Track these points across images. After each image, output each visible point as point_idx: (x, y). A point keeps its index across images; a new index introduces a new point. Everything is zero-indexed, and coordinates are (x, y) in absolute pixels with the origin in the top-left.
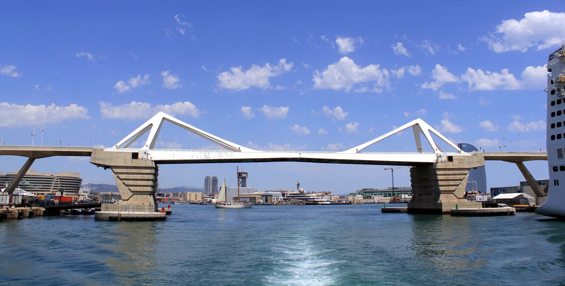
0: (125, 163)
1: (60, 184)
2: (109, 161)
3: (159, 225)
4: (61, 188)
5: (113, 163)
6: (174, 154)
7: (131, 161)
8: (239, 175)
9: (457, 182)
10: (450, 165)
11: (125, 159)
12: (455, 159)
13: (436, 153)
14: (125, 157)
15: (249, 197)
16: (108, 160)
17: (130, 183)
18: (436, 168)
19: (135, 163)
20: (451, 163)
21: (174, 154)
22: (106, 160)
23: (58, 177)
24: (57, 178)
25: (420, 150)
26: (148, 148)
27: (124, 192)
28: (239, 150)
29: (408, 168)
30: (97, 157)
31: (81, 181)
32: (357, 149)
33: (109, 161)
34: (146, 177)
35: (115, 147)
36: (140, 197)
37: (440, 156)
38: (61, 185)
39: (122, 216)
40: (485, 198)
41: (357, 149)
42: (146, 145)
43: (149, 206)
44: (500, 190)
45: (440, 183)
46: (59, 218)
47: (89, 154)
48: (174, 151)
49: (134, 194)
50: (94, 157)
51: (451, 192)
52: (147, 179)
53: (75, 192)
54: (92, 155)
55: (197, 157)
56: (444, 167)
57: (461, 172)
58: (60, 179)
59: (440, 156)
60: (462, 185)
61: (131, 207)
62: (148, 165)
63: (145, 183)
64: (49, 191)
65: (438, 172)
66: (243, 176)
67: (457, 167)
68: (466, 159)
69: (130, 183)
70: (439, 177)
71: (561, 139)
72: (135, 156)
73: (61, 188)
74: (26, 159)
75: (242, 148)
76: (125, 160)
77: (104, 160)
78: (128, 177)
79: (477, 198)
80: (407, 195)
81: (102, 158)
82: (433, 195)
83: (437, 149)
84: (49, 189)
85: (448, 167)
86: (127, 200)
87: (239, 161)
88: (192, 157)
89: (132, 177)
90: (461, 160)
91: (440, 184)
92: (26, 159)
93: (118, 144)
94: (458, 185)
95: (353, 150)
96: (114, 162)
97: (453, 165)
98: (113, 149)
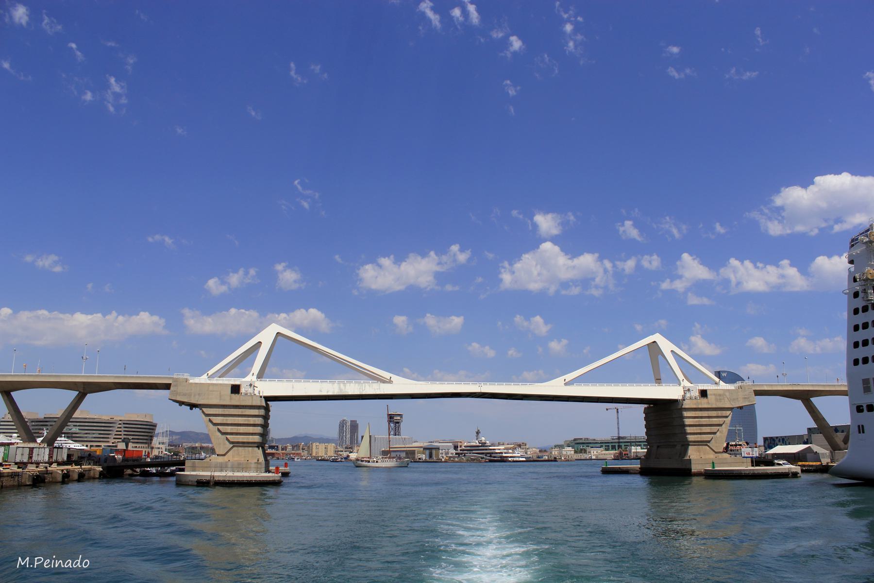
1: (125, 431)
2: (197, 397)
3: (271, 491)
4: (125, 437)
6: (293, 386)
7: (229, 398)
8: (390, 418)
9: (714, 429)
10: (704, 403)
12: (711, 395)
13: (682, 385)
14: (220, 391)
16: (195, 396)
17: (229, 429)
18: (683, 407)
19: (236, 400)
20: (704, 400)
21: (293, 386)
22: (192, 396)
23: (121, 420)
24: (120, 422)
25: (658, 381)
26: (255, 376)
27: (219, 443)
28: (390, 381)
29: (641, 408)
31: (156, 426)
32: (565, 380)
33: (197, 397)
34: (252, 420)
35: (205, 376)
36: (243, 451)
37: (689, 390)
38: (126, 433)
39: (216, 479)
40: (756, 452)
41: (565, 380)
43: (256, 464)
45: (689, 430)
47: (167, 387)
49: (233, 446)
50: (175, 391)
51: (705, 443)
53: (146, 443)
54: (172, 388)
55: (328, 392)
56: (695, 407)
57: (720, 413)
58: (124, 424)
59: (689, 390)
60: (720, 432)
61: (229, 466)
62: (254, 404)
63: (251, 429)
64: (108, 442)
65: (686, 414)
66: (396, 420)
67: (714, 406)
68: (727, 394)
69: (229, 429)
70: (687, 421)
72: (236, 389)
73: (125, 437)
74: (73, 394)
75: (395, 378)
78: (225, 420)
79: (744, 452)
81: (187, 392)
82: (678, 447)
84: (108, 438)
85: (700, 406)
86: (224, 455)
89: (230, 420)
90: (720, 395)
91: (688, 431)
92: (73, 394)
93: (211, 372)
94: (715, 433)
95: (560, 381)
96: (204, 399)
97: (708, 403)
98: (203, 379)
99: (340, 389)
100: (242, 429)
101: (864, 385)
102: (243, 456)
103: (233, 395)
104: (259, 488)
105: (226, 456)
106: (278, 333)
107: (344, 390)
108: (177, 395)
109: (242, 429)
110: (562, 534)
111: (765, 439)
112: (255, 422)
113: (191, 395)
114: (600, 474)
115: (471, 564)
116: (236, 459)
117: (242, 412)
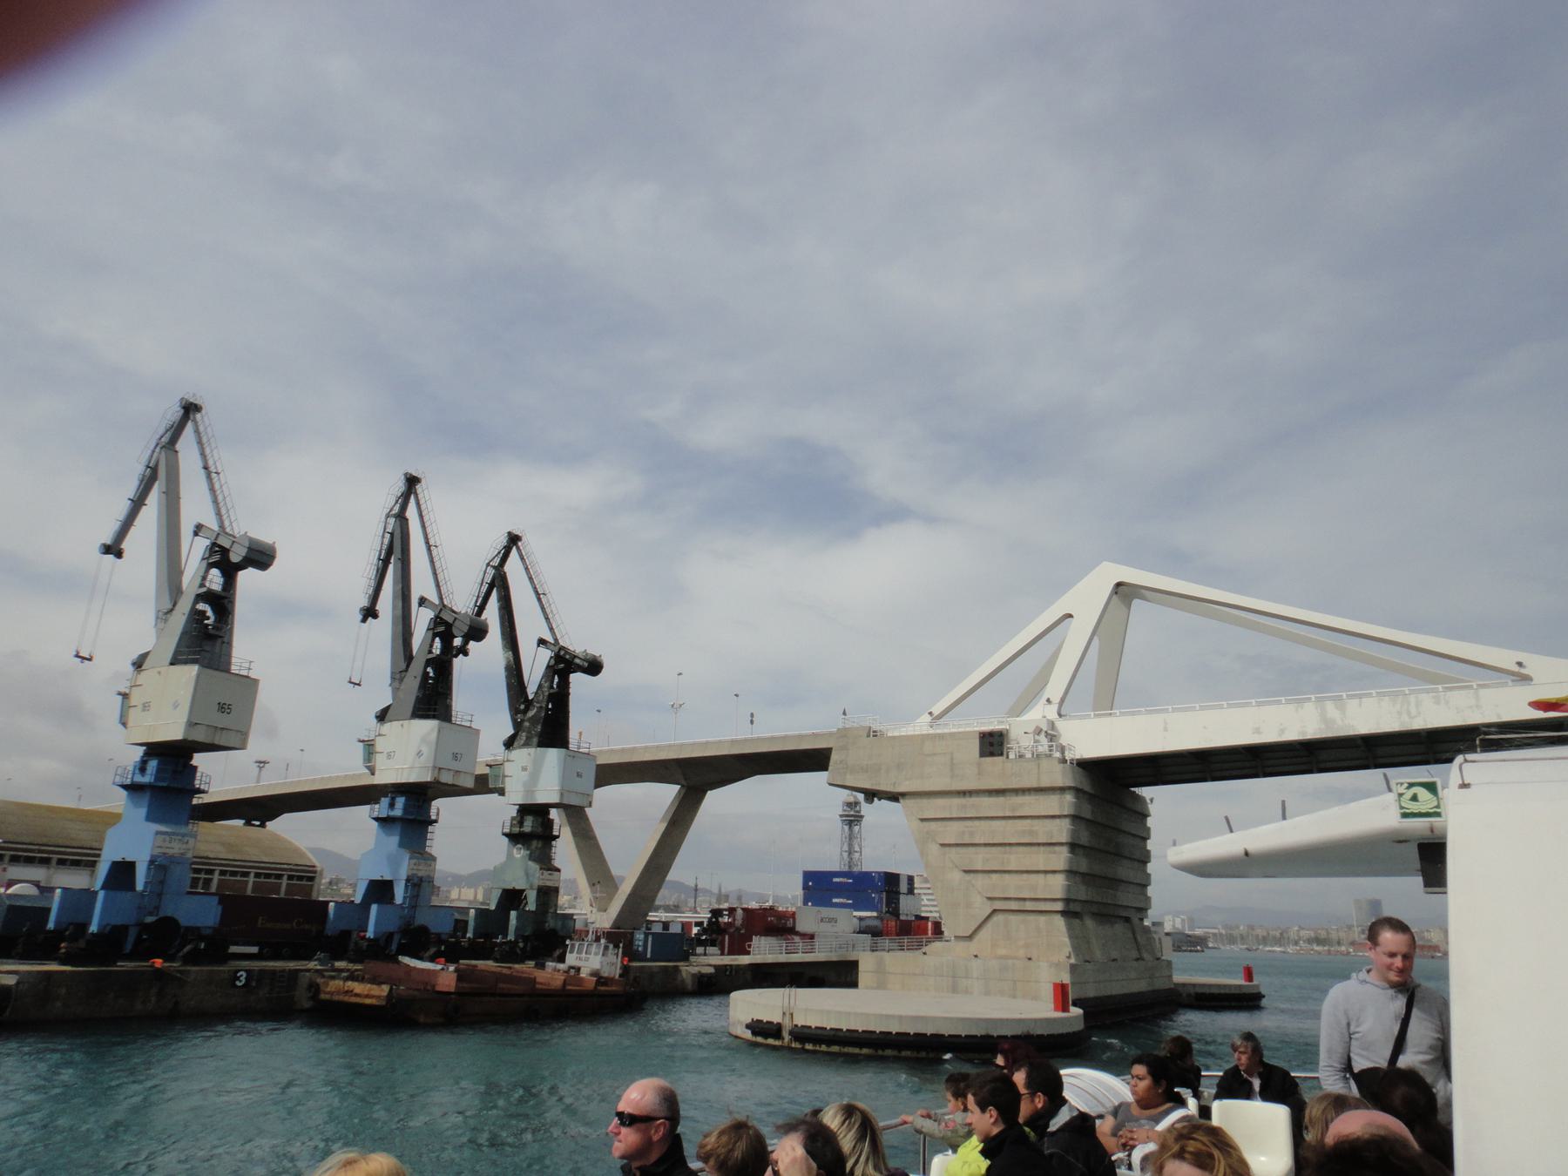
3: (86, 662)
5: (907, 783)
6: (1166, 723)
14: (952, 754)
15: (647, 949)
17: (979, 859)
19: (995, 772)
21: (1166, 723)
44: (749, 976)
55: (1282, 731)
62: (1045, 783)
63: (1040, 859)
69: (979, 859)
71: (1469, 789)
72: (993, 744)
74: (666, 794)
80: (1130, 1076)
88: (1257, 731)
89: (983, 832)
92: (666, 794)
100: (1016, 859)
104: (774, 938)
106: (1119, 585)
107: (1339, 722)
109: (1016, 859)
110: (425, 1156)
115: (1400, 988)
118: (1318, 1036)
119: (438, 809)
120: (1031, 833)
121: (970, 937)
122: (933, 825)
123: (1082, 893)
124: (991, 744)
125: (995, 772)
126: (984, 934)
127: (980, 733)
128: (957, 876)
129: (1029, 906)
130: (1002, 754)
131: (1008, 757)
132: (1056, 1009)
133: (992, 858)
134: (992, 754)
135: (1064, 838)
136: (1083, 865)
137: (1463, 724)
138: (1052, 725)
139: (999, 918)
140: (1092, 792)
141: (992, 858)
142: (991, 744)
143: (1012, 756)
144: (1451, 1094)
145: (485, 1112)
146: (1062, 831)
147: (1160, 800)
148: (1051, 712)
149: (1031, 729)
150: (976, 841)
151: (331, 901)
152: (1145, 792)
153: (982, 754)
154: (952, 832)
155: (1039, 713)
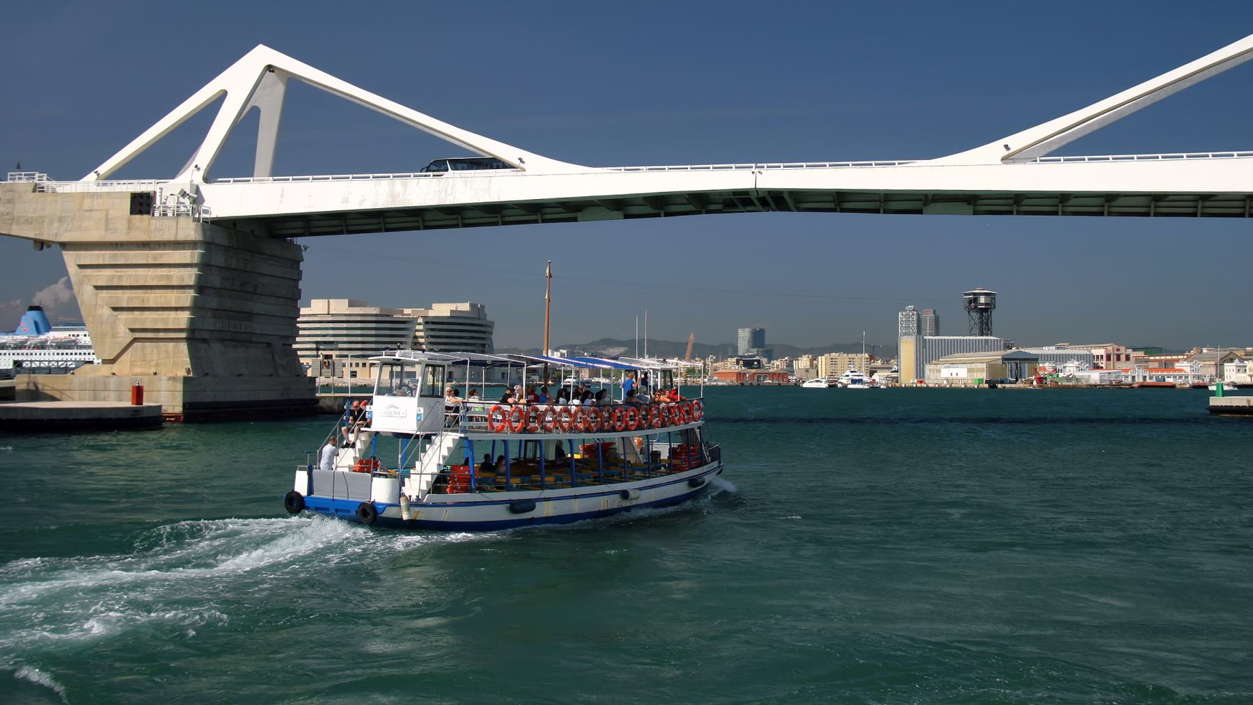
0: (107, 229)
2: (56, 225)
5: (67, 234)
7: (126, 225)
11: (109, 217)
14: (107, 210)
16: (51, 223)
17: (124, 298)
19: (145, 227)
22: (46, 224)
26: (201, 174)
28: (223, 95)
30: (15, 215)
33: (56, 225)
35: (92, 176)
36: (155, 351)
42: (192, 167)
43: (171, 382)
46: (53, 437)
48: (897, 165)
49: (135, 340)
50: (7, 214)
52: (178, 284)
61: (112, 387)
62: (181, 237)
63: (172, 298)
69: (124, 298)
75: (535, 162)
76: (107, 221)
77: (40, 221)
78: (116, 279)
81: (34, 215)
83: (96, 171)
87: (893, 205)
88: (346, 201)
95: (996, 149)
96: (70, 231)
99: (393, 195)
100: (154, 298)
101: (546, 440)
102: (154, 363)
103: (138, 217)
105: (117, 362)
108: (11, 224)
109: (154, 298)
111: (356, 372)
112: (183, 280)
113: (43, 222)
114: (1001, 163)
116: (138, 370)
117: (155, 258)
118: (109, 401)
119: (442, 175)
120: (168, 277)
121: (113, 361)
122: (89, 271)
123: (210, 324)
124: (141, 204)
125: (145, 227)
126: (126, 357)
127: (132, 194)
128: (107, 311)
129: (162, 335)
130: (148, 213)
131: (153, 215)
132: (133, 404)
133: (134, 298)
134: (141, 213)
135: (192, 282)
136: (213, 303)
137: (471, 202)
138: (197, 190)
139: (137, 345)
140: (226, 243)
141: (134, 298)
142: (141, 204)
143: (157, 214)
144: (393, 433)
145: (213, 611)
146: (189, 276)
147: (313, 248)
148: (198, 178)
149: (177, 192)
150: (124, 284)
151: (1222, 388)
152: (300, 241)
153: (132, 212)
154: (104, 277)
155: (191, 176)
